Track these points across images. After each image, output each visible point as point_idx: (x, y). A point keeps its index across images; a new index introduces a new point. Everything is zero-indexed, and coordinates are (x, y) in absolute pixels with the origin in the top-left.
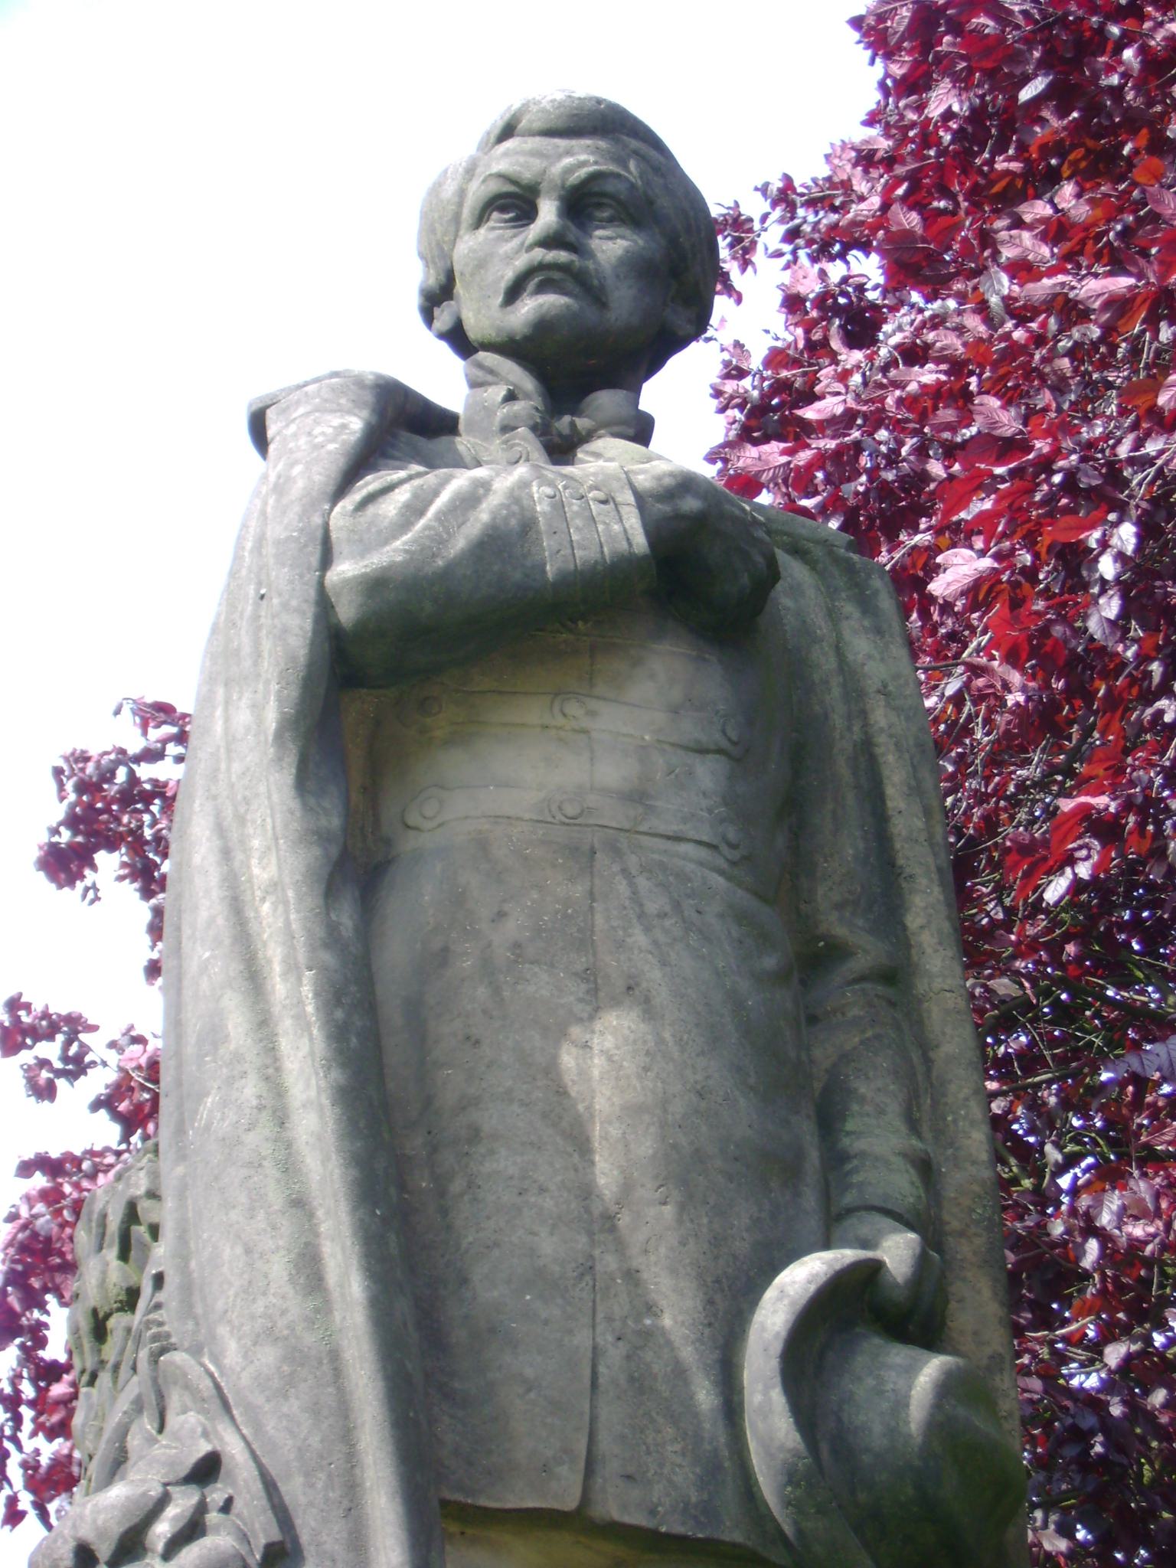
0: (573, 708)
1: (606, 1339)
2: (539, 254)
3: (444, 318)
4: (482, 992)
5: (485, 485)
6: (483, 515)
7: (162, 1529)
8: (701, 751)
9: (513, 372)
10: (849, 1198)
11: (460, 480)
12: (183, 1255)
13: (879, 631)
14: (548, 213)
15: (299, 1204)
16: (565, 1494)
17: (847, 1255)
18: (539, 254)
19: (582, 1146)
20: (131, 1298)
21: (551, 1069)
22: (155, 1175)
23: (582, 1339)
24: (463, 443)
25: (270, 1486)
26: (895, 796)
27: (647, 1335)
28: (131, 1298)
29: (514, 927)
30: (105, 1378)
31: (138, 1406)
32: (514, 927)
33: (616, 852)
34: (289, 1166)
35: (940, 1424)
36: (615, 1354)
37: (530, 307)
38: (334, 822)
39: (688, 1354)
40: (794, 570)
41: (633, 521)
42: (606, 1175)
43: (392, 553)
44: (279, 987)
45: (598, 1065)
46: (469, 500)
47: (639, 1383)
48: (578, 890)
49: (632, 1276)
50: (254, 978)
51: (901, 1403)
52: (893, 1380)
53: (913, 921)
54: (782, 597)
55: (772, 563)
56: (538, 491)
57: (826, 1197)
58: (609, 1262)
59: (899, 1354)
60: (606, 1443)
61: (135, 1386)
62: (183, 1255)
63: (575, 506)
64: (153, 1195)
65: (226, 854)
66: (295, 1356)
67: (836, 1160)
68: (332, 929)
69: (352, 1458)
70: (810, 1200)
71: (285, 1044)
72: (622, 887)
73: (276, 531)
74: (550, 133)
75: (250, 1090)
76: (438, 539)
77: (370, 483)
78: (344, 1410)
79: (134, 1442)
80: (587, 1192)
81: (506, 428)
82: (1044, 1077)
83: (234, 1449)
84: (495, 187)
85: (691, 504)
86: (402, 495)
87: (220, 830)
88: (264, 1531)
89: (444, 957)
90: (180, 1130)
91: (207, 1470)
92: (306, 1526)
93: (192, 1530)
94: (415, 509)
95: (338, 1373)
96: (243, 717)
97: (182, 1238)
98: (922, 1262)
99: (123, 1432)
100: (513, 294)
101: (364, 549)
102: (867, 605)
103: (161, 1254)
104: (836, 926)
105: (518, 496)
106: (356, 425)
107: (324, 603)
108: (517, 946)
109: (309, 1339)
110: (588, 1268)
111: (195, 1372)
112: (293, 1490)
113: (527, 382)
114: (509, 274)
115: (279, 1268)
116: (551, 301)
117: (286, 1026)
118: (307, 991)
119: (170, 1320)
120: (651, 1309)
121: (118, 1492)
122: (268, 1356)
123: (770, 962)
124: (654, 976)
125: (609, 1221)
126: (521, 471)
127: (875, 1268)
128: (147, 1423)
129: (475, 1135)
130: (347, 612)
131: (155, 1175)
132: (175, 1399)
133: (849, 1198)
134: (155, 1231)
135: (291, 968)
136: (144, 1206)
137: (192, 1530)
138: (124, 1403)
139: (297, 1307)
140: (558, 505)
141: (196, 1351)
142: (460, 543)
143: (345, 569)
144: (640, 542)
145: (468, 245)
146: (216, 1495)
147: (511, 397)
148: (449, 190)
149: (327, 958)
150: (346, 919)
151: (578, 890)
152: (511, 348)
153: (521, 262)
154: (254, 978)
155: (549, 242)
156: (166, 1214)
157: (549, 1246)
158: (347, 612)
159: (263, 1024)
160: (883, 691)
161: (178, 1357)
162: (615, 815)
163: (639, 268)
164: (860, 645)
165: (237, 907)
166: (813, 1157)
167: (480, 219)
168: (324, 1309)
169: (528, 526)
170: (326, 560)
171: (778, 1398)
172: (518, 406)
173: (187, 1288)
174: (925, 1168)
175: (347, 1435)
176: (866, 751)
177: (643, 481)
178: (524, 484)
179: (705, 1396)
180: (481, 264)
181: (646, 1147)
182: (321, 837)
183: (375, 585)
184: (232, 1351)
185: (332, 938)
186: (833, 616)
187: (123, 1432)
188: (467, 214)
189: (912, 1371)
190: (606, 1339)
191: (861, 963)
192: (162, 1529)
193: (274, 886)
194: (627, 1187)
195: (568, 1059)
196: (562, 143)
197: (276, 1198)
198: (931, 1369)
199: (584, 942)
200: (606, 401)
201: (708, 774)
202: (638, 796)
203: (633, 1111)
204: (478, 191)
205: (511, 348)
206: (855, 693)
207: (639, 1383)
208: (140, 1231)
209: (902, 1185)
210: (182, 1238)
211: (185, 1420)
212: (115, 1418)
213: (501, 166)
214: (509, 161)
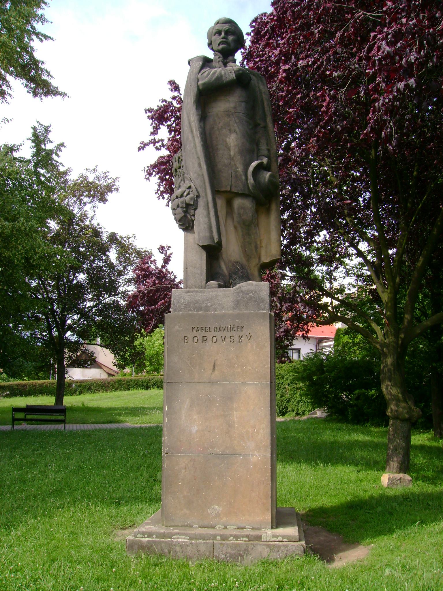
0: (227, 97)
1: (233, 172)
2: (222, 40)
3: (211, 47)
4: (218, 132)
5: (216, 71)
6: (216, 75)
7: (185, 194)
8: (243, 102)
9: (219, 54)
10: (260, 154)
11: (213, 70)
12: (185, 164)
13: (264, 85)
14: (223, 34)
15: (198, 158)
16: (228, 189)
17: (259, 161)
18: (222, 40)
19: (229, 149)
20: (180, 168)
21: (226, 141)
22: (181, 154)
23: (230, 172)
24: (214, 64)
25: (196, 189)
26: (266, 106)
27: (237, 171)
28: (180, 168)
29: (221, 124)
30: (177, 176)
31: (181, 180)
32: (221, 124)
33: (233, 115)
34: (197, 154)
35: (270, 180)
36: (233, 173)
37: (221, 46)
38: (200, 113)
39: (242, 173)
40: (253, 78)
41: (234, 75)
42: (232, 153)
43: (206, 80)
44: (195, 132)
45: (231, 140)
46: (214, 73)
47: (236, 176)
48: (228, 120)
49: (235, 164)
50: (192, 132)
51: (265, 178)
52: (264, 175)
53: (268, 121)
54: (252, 82)
55: (250, 78)
56: (223, 71)
57: (257, 154)
58: (233, 163)
59: (265, 172)
60: (233, 183)
61: (181, 178)
62: (185, 164)
63: (227, 73)
64: (181, 156)
65: (188, 117)
66: (198, 175)
67: (259, 150)
68: (200, 126)
69: (205, 186)
70: (255, 155)
71: (196, 139)
72: (233, 119)
73: (192, 77)
74: (223, 23)
75: (192, 145)
76: (211, 78)
77: (203, 71)
78: (204, 180)
79: (181, 184)
80: (230, 155)
81: (219, 62)
82: (181, 540)
83: (192, 185)
84: (216, 31)
85: (241, 72)
86: (207, 73)
87: (187, 114)
88: (196, 194)
89: (213, 128)
90: (184, 149)
91: (190, 187)
92: (201, 193)
93: (188, 194)
94: (208, 74)
95: (203, 177)
96: (189, 100)
97: (185, 161)
98: (268, 162)
99: (180, 183)
100: (219, 45)
101: (202, 80)
102: (262, 82)
103: (183, 163)
104: (259, 121)
105: (220, 73)
106: (201, 63)
107: (198, 86)
108: (222, 127)
109: (200, 173)
110: (230, 164)
111: (188, 177)
112: (199, 189)
113: (221, 56)
114: (218, 42)
115: (196, 165)
116: (223, 46)
117: (196, 137)
118: (198, 133)
119: (184, 171)
120: (237, 168)
121: (180, 190)
122: (196, 175)
123: (251, 127)
124: (237, 130)
125: (233, 158)
126: (221, 69)
127: (263, 162)
128: (183, 182)
129: (217, 149)
130: (201, 88)
131: (181, 154)
132: (185, 180)
133: (260, 154)
134: (182, 160)
135: (196, 131)
136: (180, 157)
137: (188, 194)
138: (180, 180)
139: (198, 169)
140: (225, 73)
141: (188, 174)
142: (214, 79)
143: (200, 82)
144: (235, 77)
145: (214, 38)
146: (191, 190)
147: (219, 58)
148: (211, 31)
149: (200, 129)
150: (202, 124)
151: (228, 120)
152: (219, 51)
153: (220, 41)
154: (192, 132)
155: (223, 38)
156: (183, 158)
157: (226, 161)
158: (201, 88)
159: (193, 137)
160: (264, 92)
161: (185, 175)
162: (232, 110)
163: (234, 41)
164: (262, 87)
165: (190, 123)
166: (256, 149)
167: (215, 35)
168: (202, 169)
169: (221, 76)
170: (198, 82)
171: (252, 178)
172: (220, 59)
173: (186, 167)
174: (269, 150)
175: (205, 183)
176: (262, 100)
177: (235, 69)
178: (221, 71)
179: (243, 178)
180: (215, 41)
181: (237, 150)
182: (198, 115)
183: (204, 84)
184: (192, 174)
185: (201, 127)
186: (258, 83)
187: (180, 183)
188: (213, 34)
189: (266, 174)
190: (233, 172)
191: (262, 126)
192: (185, 194)
193: (194, 121)
194: (235, 155)
195: (228, 140)
196: (224, 25)
197: (196, 157)
198: (269, 174)
199: (229, 126)
200: (230, 58)
201: (243, 105)
202: (235, 108)
203: (235, 146)
204: (214, 31)
205: (219, 51)
206: (261, 93)
207: (236, 176)
208: (180, 160)
209: (266, 152)
210: (185, 161)
211: (187, 182)
212: (179, 182)
213: (217, 28)
214: (219, 27)
